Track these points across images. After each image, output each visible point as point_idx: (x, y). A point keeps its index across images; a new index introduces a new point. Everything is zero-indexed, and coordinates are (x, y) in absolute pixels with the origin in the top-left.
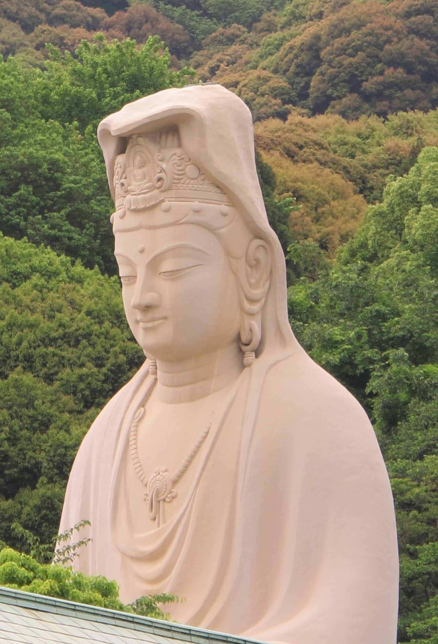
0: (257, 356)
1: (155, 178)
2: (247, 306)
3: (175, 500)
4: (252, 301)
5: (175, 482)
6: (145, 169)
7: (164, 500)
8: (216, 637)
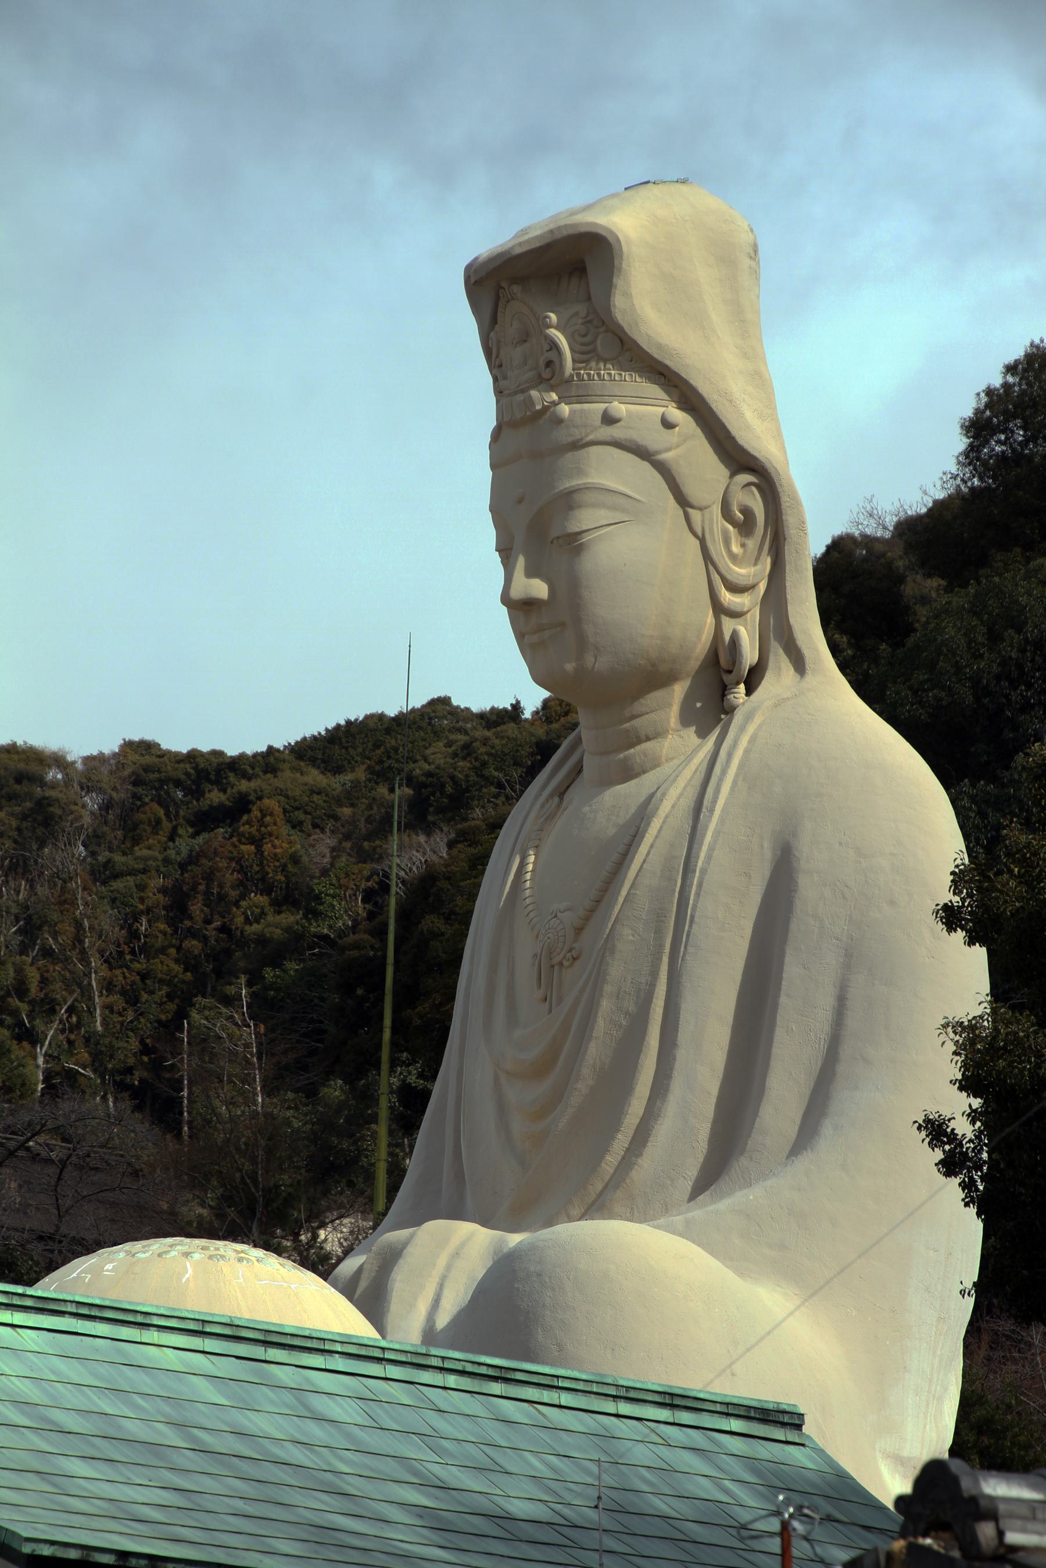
0: (749, 692)
1: (542, 364)
2: (727, 597)
3: (577, 963)
4: (735, 589)
5: (579, 930)
6: (527, 345)
7: (561, 964)
8: (309, 1344)
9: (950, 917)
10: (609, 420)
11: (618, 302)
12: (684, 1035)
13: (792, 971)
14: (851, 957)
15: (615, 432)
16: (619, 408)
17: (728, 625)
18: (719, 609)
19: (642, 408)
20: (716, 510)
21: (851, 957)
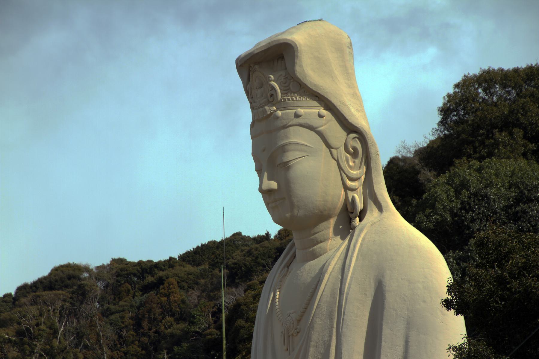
2: (349, 183)
10: (297, 116)
11: (298, 69)
13: (386, 331)
14: (409, 325)
16: (301, 111)
17: (350, 194)
18: (346, 188)
19: (310, 111)
20: (342, 149)
21: (409, 325)
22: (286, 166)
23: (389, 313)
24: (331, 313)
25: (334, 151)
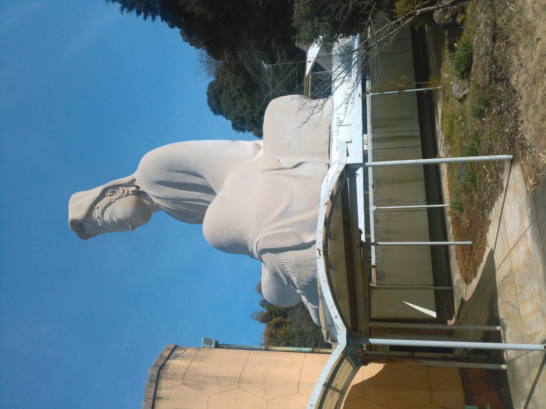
2: (125, 194)
9: (260, 135)
10: (99, 218)
11: (80, 219)
12: (192, 198)
13: (175, 180)
14: (171, 170)
15: (100, 217)
16: (97, 217)
17: (130, 193)
18: (128, 194)
19: (97, 213)
20: (111, 197)
21: (171, 170)
22: (119, 221)
23: (168, 179)
24: (174, 203)
25: (112, 201)
